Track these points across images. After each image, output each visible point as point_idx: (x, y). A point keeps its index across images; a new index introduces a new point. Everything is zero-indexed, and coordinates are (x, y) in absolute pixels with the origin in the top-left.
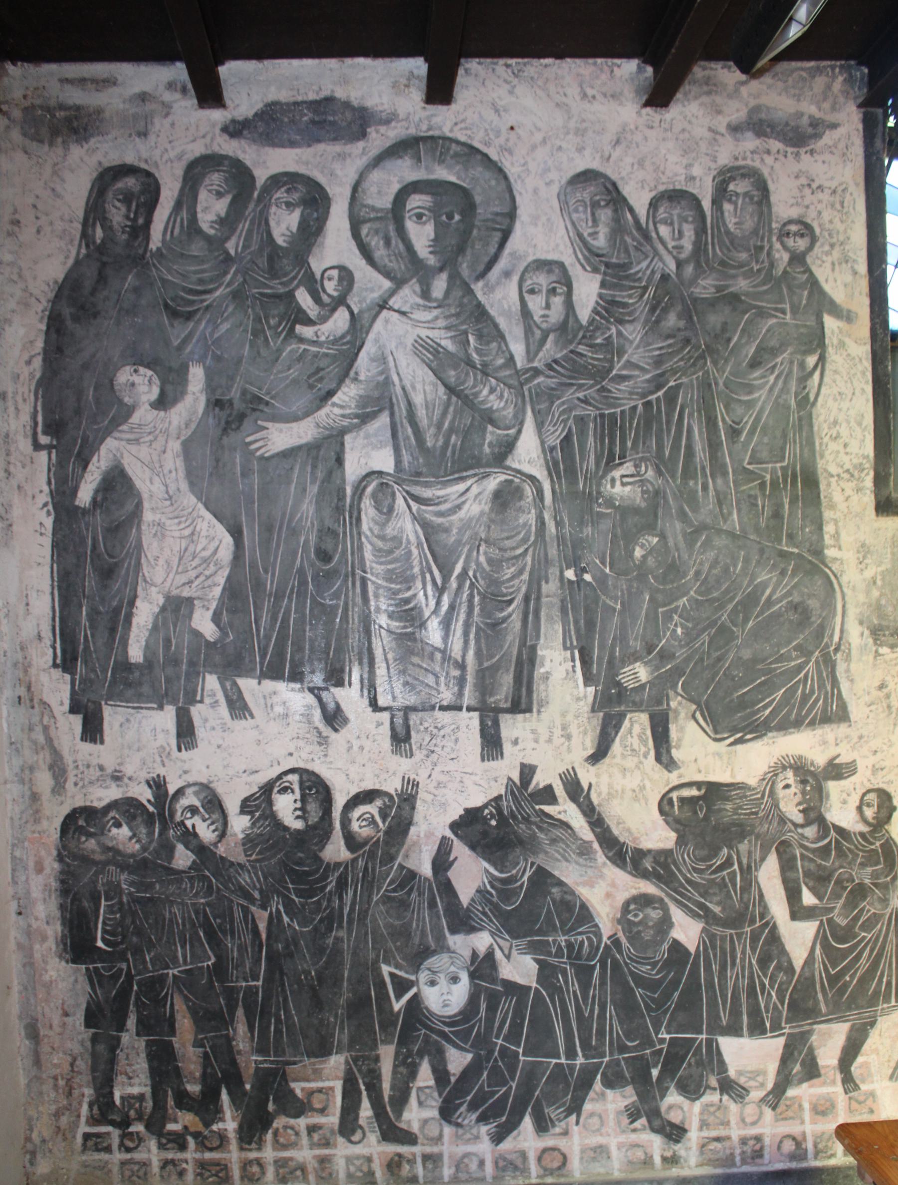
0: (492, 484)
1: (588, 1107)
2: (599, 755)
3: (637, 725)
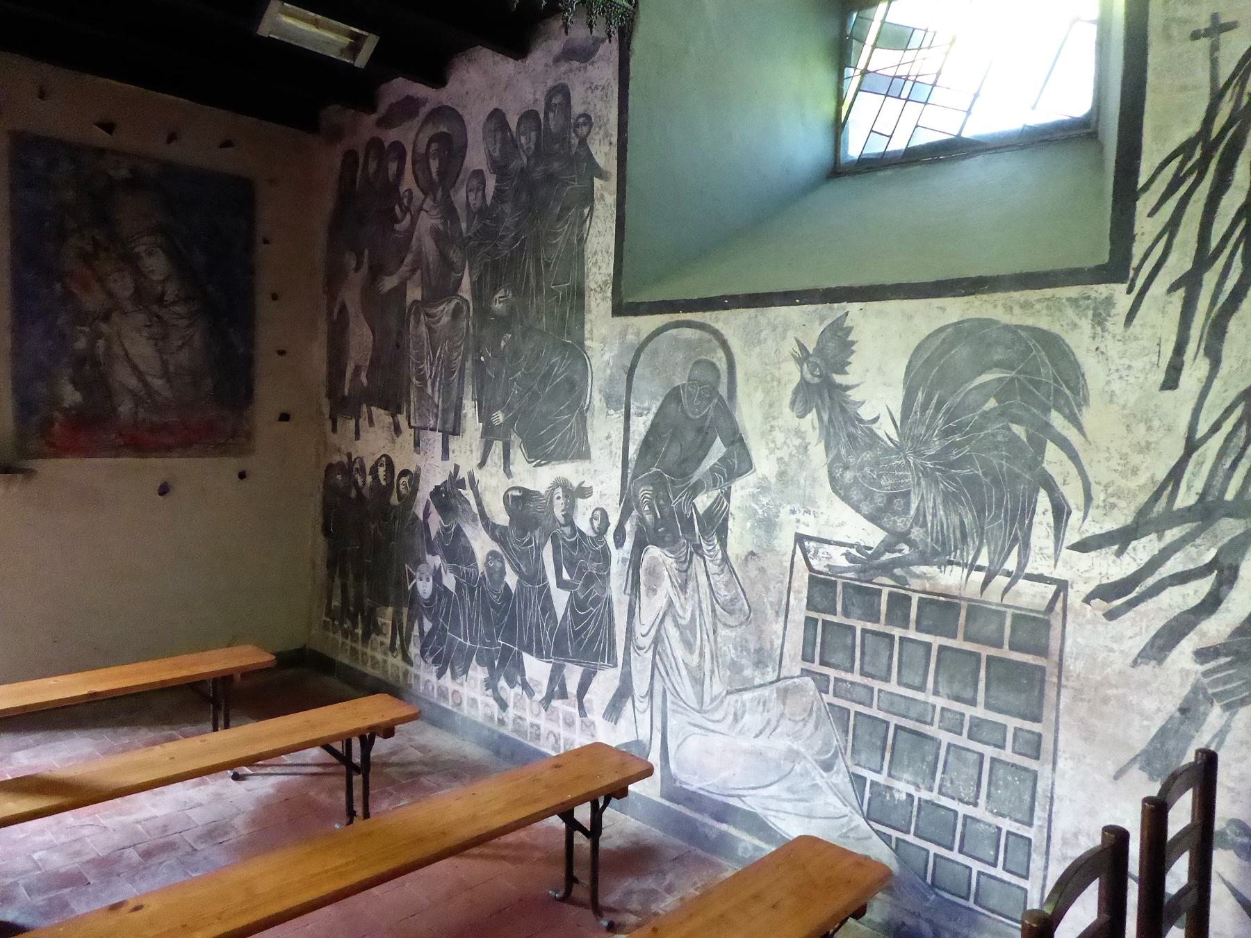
0: (452, 305)
1: (470, 672)
2: (482, 465)
3: (498, 447)
